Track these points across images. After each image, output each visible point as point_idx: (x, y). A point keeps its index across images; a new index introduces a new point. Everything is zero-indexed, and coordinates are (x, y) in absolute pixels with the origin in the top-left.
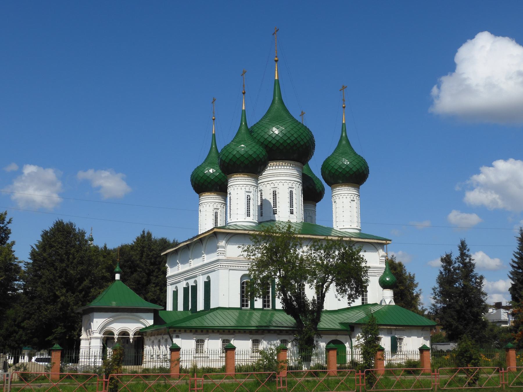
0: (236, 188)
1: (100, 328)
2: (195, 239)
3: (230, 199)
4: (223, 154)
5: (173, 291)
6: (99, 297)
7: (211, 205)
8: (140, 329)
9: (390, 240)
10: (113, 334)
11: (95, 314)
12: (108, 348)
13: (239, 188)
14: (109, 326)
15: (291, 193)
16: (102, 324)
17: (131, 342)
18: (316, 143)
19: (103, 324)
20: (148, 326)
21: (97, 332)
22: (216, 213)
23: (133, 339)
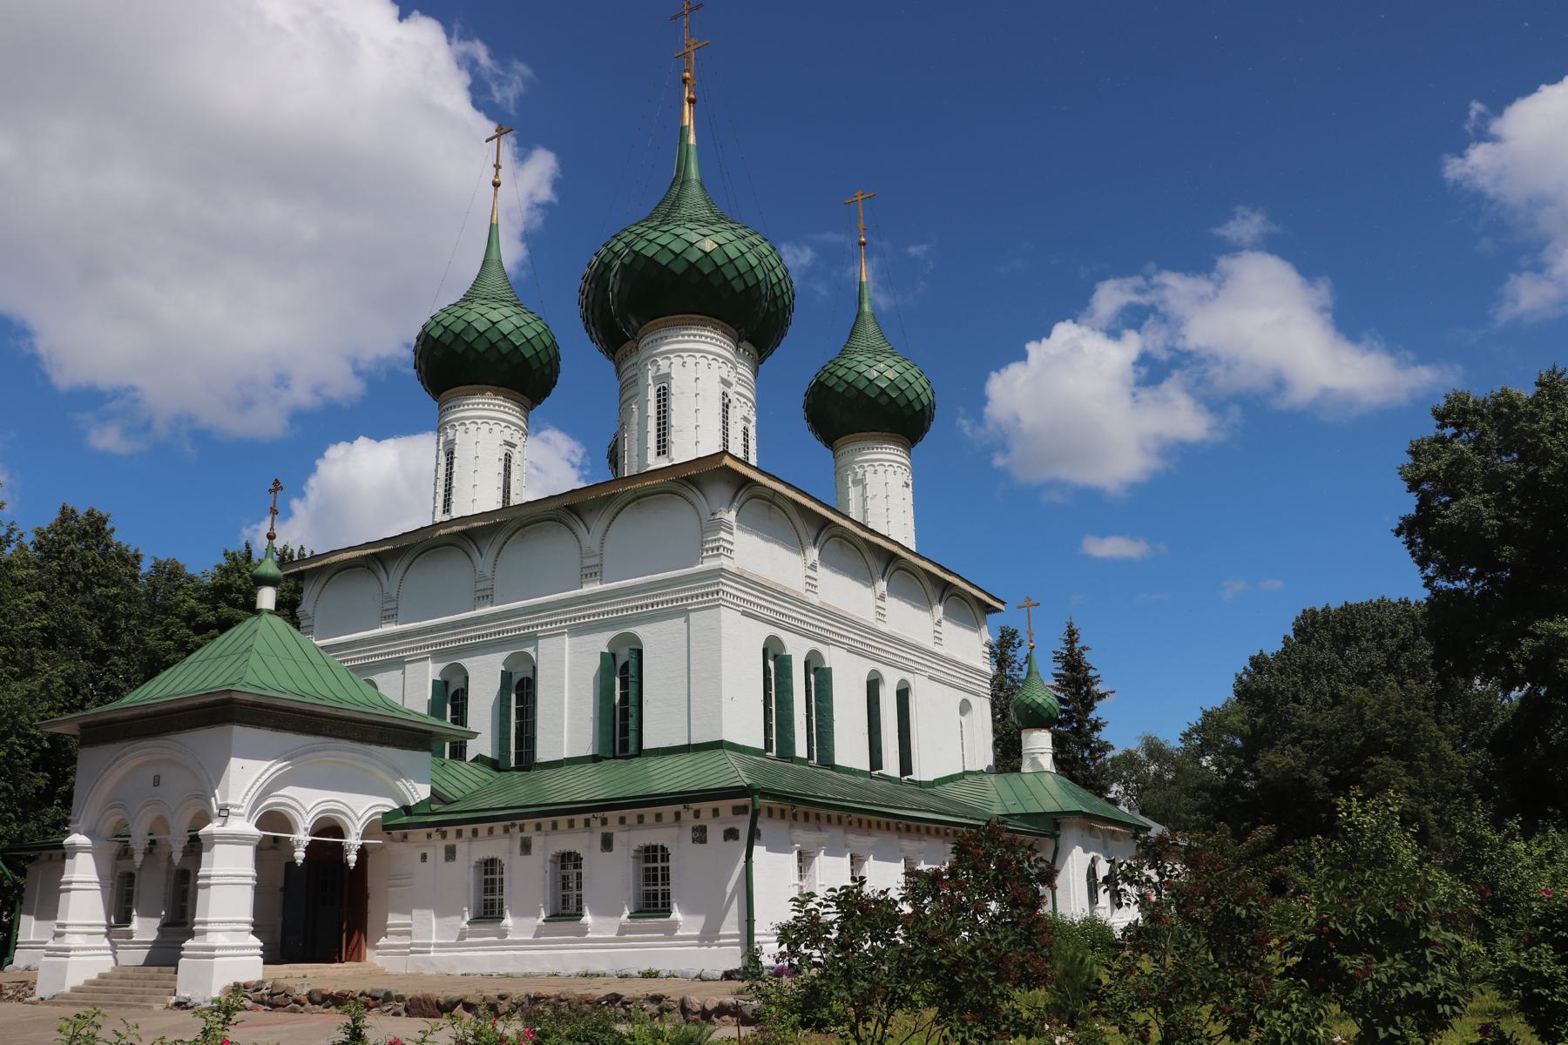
0: (690, 361)
1: (258, 793)
2: (442, 532)
3: (663, 396)
4: (438, 323)
5: (602, 653)
6: (179, 668)
7: (497, 429)
8: (385, 814)
9: (1003, 603)
11: (239, 733)
12: (919, 868)
13: (485, 428)
14: (280, 792)
16: (261, 781)
17: (352, 865)
18: (791, 330)
19: (264, 778)
20: (412, 803)
21: (241, 811)
22: (508, 459)
23: (308, 849)
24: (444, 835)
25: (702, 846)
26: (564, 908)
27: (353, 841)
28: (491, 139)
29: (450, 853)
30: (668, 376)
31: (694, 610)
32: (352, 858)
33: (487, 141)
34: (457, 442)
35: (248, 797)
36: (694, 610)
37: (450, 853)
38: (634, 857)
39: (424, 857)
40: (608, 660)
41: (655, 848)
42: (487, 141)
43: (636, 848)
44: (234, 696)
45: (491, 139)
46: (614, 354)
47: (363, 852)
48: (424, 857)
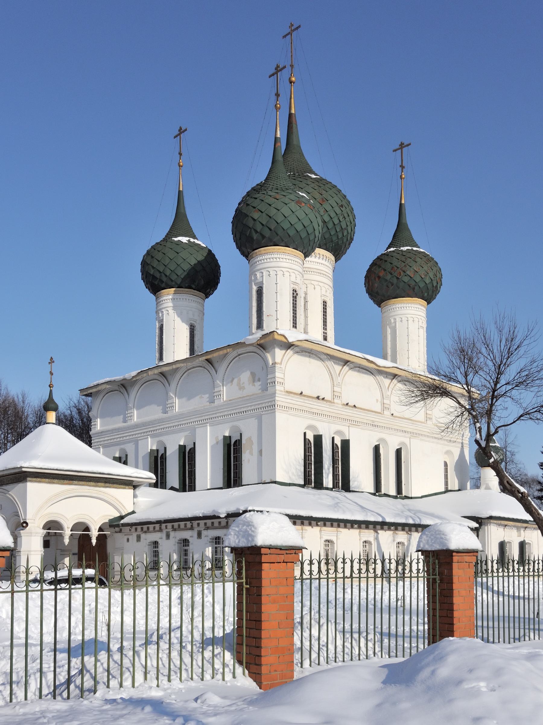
10: (87, 529)
15: (325, 303)
24: (136, 529)
25: (200, 540)
26: (186, 565)
27: (94, 534)
28: (273, 75)
29: (139, 538)
30: (262, 283)
31: (140, 440)
32: (94, 541)
33: (270, 77)
34: (264, 282)
35: (115, 501)
36: (140, 440)
37: (139, 538)
38: (178, 543)
39: (128, 540)
40: (227, 440)
41: (219, 537)
42: (270, 77)
43: (211, 538)
44: (24, 469)
45: (273, 75)
46: (155, 294)
47: (99, 538)
48: (128, 540)
